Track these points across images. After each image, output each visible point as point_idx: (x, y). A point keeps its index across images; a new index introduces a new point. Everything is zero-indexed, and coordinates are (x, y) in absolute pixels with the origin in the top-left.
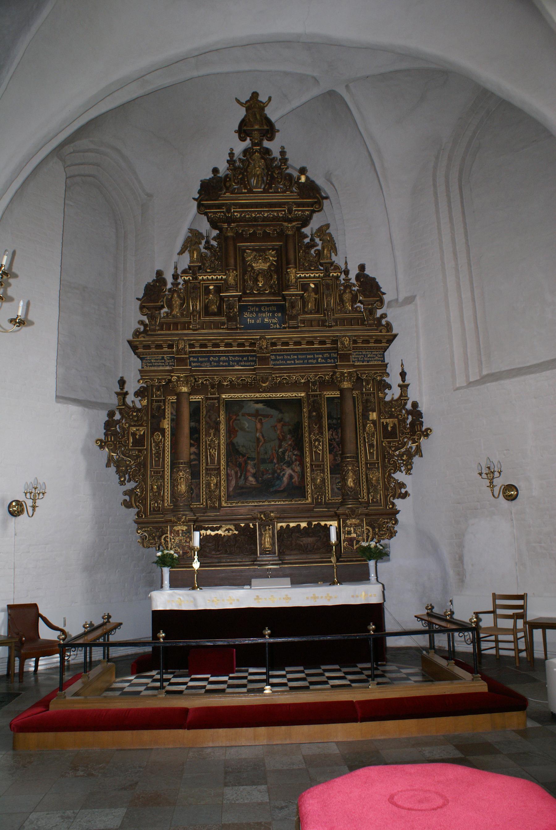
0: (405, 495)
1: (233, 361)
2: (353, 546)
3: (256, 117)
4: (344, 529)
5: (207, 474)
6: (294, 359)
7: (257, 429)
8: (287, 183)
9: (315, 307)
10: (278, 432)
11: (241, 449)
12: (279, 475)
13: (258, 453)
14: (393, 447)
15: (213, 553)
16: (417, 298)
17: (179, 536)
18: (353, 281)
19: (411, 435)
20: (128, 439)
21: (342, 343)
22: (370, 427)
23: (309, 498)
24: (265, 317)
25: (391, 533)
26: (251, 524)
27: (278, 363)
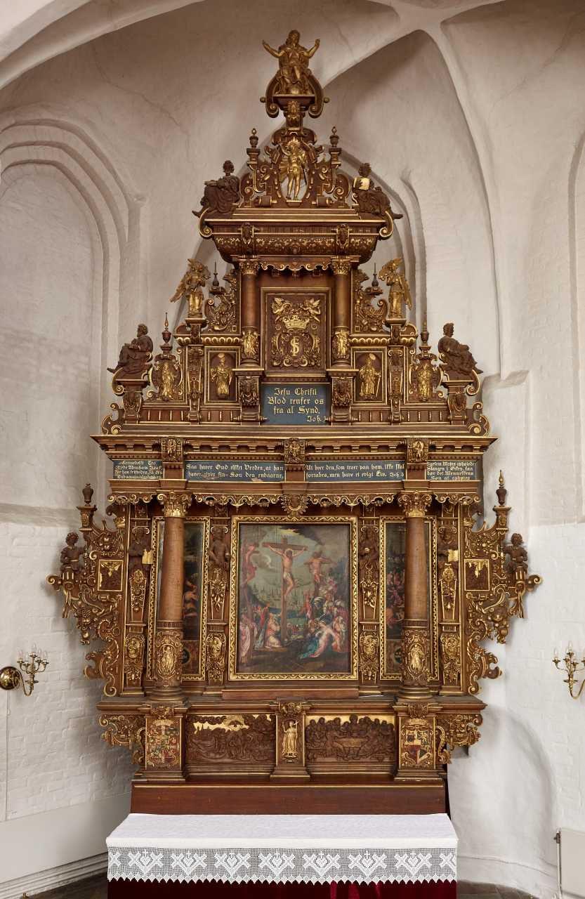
0: (495, 674)
1: (249, 472)
2: (415, 758)
3: (295, 77)
4: (405, 732)
5: (208, 632)
6: (340, 472)
7: (284, 567)
8: (339, 190)
9: (375, 391)
10: (315, 572)
11: (259, 596)
12: (313, 636)
13: (285, 602)
14: (481, 601)
15: (212, 755)
16: (531, 375)
17: (160, 734)
18: (434, 350)
19: (508, 585)
20: (97, 578)
21: (415, 452)
22: (448, 571)
23: (355, 673)
24: (300, 405)
25: (473, 736)
26: (268, 716)
27: (317, 476)
